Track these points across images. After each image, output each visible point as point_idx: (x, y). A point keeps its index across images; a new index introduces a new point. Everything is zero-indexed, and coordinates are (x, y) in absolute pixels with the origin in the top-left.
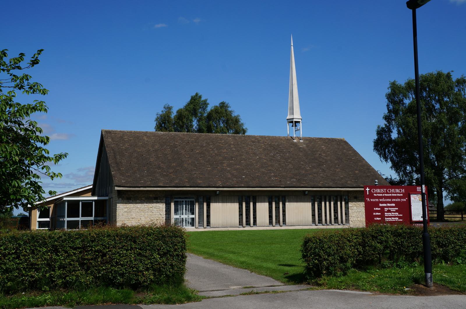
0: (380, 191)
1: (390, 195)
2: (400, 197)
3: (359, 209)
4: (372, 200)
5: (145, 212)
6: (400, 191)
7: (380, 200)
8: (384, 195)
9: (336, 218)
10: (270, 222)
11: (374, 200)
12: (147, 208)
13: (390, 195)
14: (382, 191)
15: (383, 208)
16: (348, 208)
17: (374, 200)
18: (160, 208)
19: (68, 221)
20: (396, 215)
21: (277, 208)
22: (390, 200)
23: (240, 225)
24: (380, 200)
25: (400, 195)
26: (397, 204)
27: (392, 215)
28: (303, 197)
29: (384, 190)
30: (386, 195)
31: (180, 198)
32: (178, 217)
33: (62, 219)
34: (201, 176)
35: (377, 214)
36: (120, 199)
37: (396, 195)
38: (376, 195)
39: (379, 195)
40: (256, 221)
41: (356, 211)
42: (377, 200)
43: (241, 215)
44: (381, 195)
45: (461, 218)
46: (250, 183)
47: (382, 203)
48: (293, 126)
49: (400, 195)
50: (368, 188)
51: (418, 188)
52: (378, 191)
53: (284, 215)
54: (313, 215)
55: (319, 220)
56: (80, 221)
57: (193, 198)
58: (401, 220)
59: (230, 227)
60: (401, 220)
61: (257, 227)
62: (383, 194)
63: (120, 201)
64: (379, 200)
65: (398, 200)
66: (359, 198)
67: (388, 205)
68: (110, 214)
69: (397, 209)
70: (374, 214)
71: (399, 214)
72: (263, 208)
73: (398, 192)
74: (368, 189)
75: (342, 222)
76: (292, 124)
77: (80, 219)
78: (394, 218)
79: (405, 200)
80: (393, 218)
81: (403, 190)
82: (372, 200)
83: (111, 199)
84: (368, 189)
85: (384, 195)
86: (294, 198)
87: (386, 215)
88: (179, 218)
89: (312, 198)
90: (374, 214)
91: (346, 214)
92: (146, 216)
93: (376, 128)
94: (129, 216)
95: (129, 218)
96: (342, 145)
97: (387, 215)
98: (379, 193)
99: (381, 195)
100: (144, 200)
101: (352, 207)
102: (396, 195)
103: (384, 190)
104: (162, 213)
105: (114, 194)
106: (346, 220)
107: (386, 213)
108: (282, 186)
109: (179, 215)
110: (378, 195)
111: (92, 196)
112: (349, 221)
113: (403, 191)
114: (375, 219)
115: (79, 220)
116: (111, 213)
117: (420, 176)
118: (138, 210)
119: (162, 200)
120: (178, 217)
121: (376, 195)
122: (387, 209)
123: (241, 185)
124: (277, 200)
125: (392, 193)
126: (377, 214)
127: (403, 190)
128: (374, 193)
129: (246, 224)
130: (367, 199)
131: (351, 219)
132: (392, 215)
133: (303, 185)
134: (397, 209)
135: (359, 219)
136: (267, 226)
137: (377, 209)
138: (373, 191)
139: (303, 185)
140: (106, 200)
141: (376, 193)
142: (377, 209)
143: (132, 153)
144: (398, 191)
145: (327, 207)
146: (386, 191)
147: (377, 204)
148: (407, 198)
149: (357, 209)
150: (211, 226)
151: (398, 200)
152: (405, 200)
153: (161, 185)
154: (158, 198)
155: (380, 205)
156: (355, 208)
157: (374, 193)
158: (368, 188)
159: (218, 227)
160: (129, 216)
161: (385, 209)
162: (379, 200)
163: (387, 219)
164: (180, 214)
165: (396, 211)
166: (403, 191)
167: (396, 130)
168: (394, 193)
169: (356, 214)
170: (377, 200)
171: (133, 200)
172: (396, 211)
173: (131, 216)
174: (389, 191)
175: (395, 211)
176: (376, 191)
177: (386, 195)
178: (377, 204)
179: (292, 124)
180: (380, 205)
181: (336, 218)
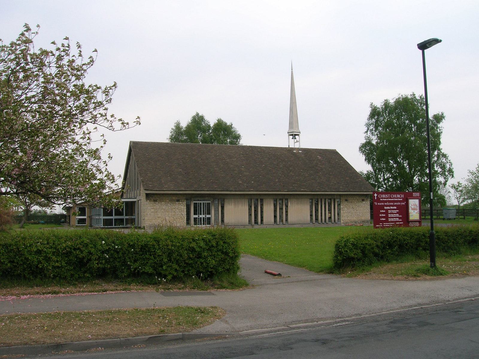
0: (385, 196)
1: (393, 199)
2: (400, 201)
4: (378, 204)
5: (169, 212)
6: (401, 196)
7: (385, 204)
8: (388, 200)
9: (317, 219)
10: (274, 221)
11: (380, 204)
12: (171, 209)
13: (393, 199)
14: (387, 196)
15: (387, 210)
16: (340, 210)
17: (380, 204)
18: (182, 209)
19: (104, 219)
20: (397, 216)
21: (281, 209)
22: (392, 204)
23: (274, 223)
24: (385, 204)
25: (400, 200)
26: (398, 207)
27: (394, 216)
29: (388, 196)
30: (390, 199)
31: (198, 200)
32: (196, 216)
33: (98, 217)
34: (216, 182)
35: (383, 215)
36: (148, 201)
37: (397, 200)
38: (382, 200)
39: (384, 200)
40: (263, 220)
41: (347, 211)
42: (383, 204)
43: (250, 215)
44: (386, 200)
47: (387, 206)
48: (293, 139)
49: (400, 200)
50: (376, 194)
51: (414, 193)
52: (384, 196)
53: (287, 215)
54: (311, 215)
55: (255, 221)
56: (133, 217)
57: (210, 201)
58: (400, 220)
60: (400, 220)
62: (387, 198)
63: (148, 203)
64: (384, 204)
65: (399, 204)
67: (391, 207)
68: (138, 214)
69: (398, 211)
70: (380, 215)
71: (399, 215)
72: (268, 210)
73: (399, 197)
74: (376, 195)
76: (292, 136)
77: (202, 216)
78: (395, 219)
79: (404, 204)
80: (394, 219)
81: (402, 195)
82: (378, 204)
83: (140, 201)
84: (376, 195)
85: (388, 200)
86: (295, 200)
87: (389, 216)
88: (200, 215)
89: (311, 201)
90: (380, 215)
91: (338, 214)
92: (170, 216)
93: (194, 114)
94: (156, 216)
95: (156, 217)
96: (334, 154)
97: (390, 216)
98: (384, 198)
99: (386, 200)
100: (168, 202)
101: (343, 209)
102: (397, 200)
103: (388, 196)
104: (183, 213)
105: (142, 196)
106: (338, 219)
107: (389, 215)
109: (198, 215)
110: (383, 199)
112: (340, 220)
113: (403, 196)
114: (381, 219)
115: (124, 219)
116: (140, 212)
118: (163, 211)
119: (184, 202)
120: (196, 216)
121: (382, 200)
122: (390, 211)
123: (251, 189)
124: (280, 202)
125: (394, 198)
126: (383, 215)
127: (402, 195)
128: (381, 198)
129: (255, 223)
130: (375, 203)
132: (394, 216)
133: (303, 189)
134: (398, 211)
137: (382, 211)
138: (380, 196)
139: (303, 189)
140: (135, 202)
141: (382, 198)
142: (382, 211)
144: (398, 196)
145: (323, 209)
146: (390, 196)
147: (382, 207)
148: (405, 202)
151: (399, 204)
152: (404, 204)
153: (183, 189)
154: (180, 201)
155: (385, 208)
156: (346, 209)
157: (381, 198)
158: (376, 194)
160: (156, 216)
161: (389, 211)
162: (384, 204)
163: (390, 219)
165: (397, 213)
166: (403, 196)
167: (444, 153)
168: (396, 198)
170: (383, 204)
171: (158, 202)
172: (397, 213)
173: (157, 216)
174: (392, 196)
175: (396, 212)
176: (382, 197)
177: (390, 199)
178: (382, 207)
179: (292, 136)
180: (385, 208)
181: (317, 219)
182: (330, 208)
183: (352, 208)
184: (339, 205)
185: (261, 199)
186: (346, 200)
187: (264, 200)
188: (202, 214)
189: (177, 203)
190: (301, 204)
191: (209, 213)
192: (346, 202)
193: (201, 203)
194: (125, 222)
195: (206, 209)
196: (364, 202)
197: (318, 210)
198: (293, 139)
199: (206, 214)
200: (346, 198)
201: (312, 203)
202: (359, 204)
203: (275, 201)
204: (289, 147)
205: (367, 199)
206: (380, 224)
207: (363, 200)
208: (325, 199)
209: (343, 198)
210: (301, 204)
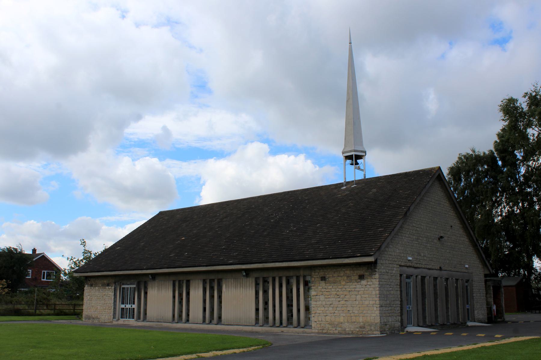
3: (328, 299)
5: (100, 300)
28: (244, 279)
45: (76, 309)
46: (366, 250)
59: (164, 322)
61: (190, 323)
66: (330, 279)
75: (281, 323)
86: (232, 281)
96: (161, 213)
108: (203, 265)
111: (359, 275)
117: (97, 255)
131: (314, 318)
135: (328, 318)
136: (200, 324)
143: (322, 208)
149: (326, 300)
150: (223, 323)
159: (153, 321)
164: (125, 304)
169: (323, 309)
181: (266, 318)
182: (290, 295)
183: (336, 296)
184: (146, 288)
185: (179, 281)
186: (323, 279)
187: (191, 282)
188: (128, 308)
189: (107, 288)
190: (241, 288)
191: (123, 309)
192: (323, 283)
193: (128, 288)
194: (513, 340)
195: (132, 296)
196: (364, 282)
197: (182, 299)
198: (352, 164)
199: (131, 308)
200: (322, 274)
201: (257, 284)
202: (351, 287)
203: (204, 282)
204: (365, 177)
205: (371, 275)
206: (496, 336)
207: (361, 277)
208: (280, 279)
209: (317, 274)
210: (241, 288)
